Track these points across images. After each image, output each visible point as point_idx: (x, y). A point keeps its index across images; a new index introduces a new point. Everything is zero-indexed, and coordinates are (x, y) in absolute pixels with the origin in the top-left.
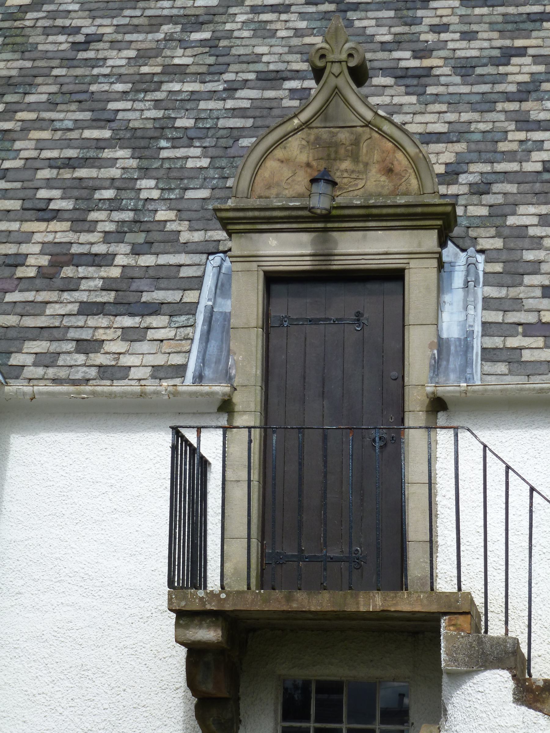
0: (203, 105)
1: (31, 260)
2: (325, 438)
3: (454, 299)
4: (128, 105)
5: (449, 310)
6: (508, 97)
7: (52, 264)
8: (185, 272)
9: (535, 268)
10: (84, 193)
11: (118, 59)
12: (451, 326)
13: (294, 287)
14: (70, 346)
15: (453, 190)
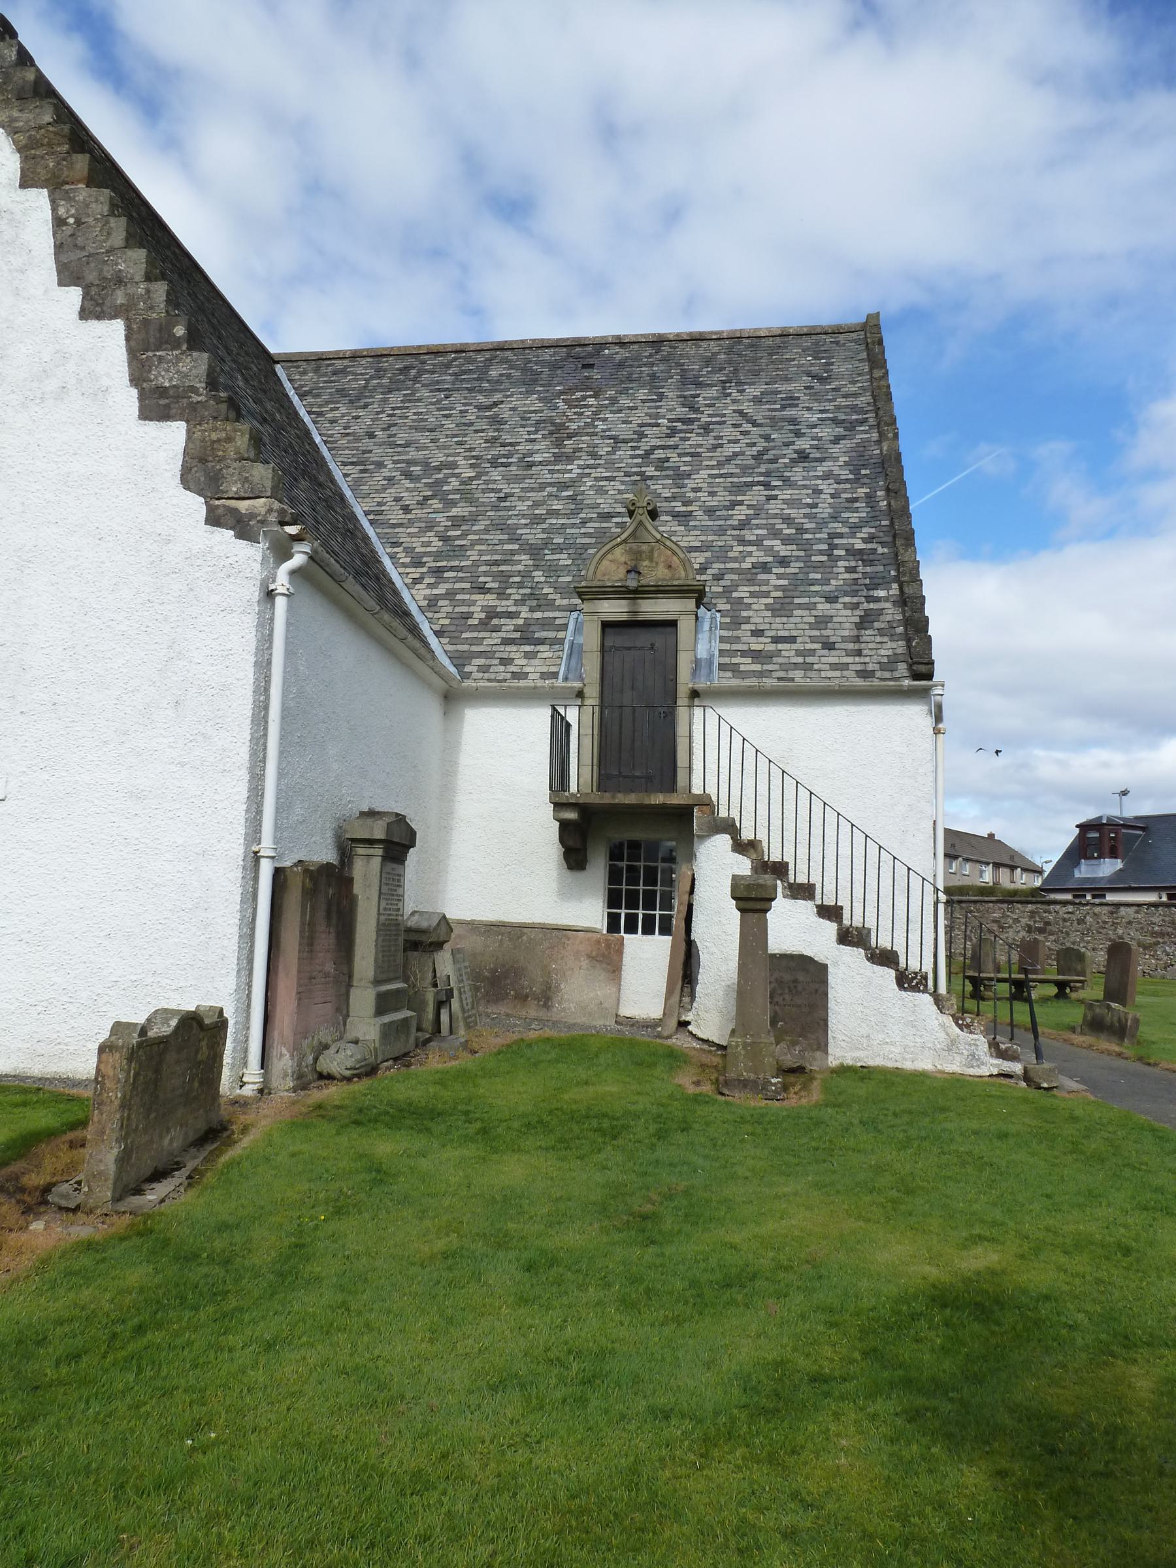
0: (568, 531)
1: (476, 615)
2: (634, 712)
3: (704, 637)
4: (528, 531)
5: (701, 643)
6: (734, 528)
7: (487, 617)
8: (558, 622)
9: (747, 620)
10: (504, 579)
11: (522, 506)
12: (702, 652)
13: (617, 630)
14: (497, 662)
15: (703, 577)
